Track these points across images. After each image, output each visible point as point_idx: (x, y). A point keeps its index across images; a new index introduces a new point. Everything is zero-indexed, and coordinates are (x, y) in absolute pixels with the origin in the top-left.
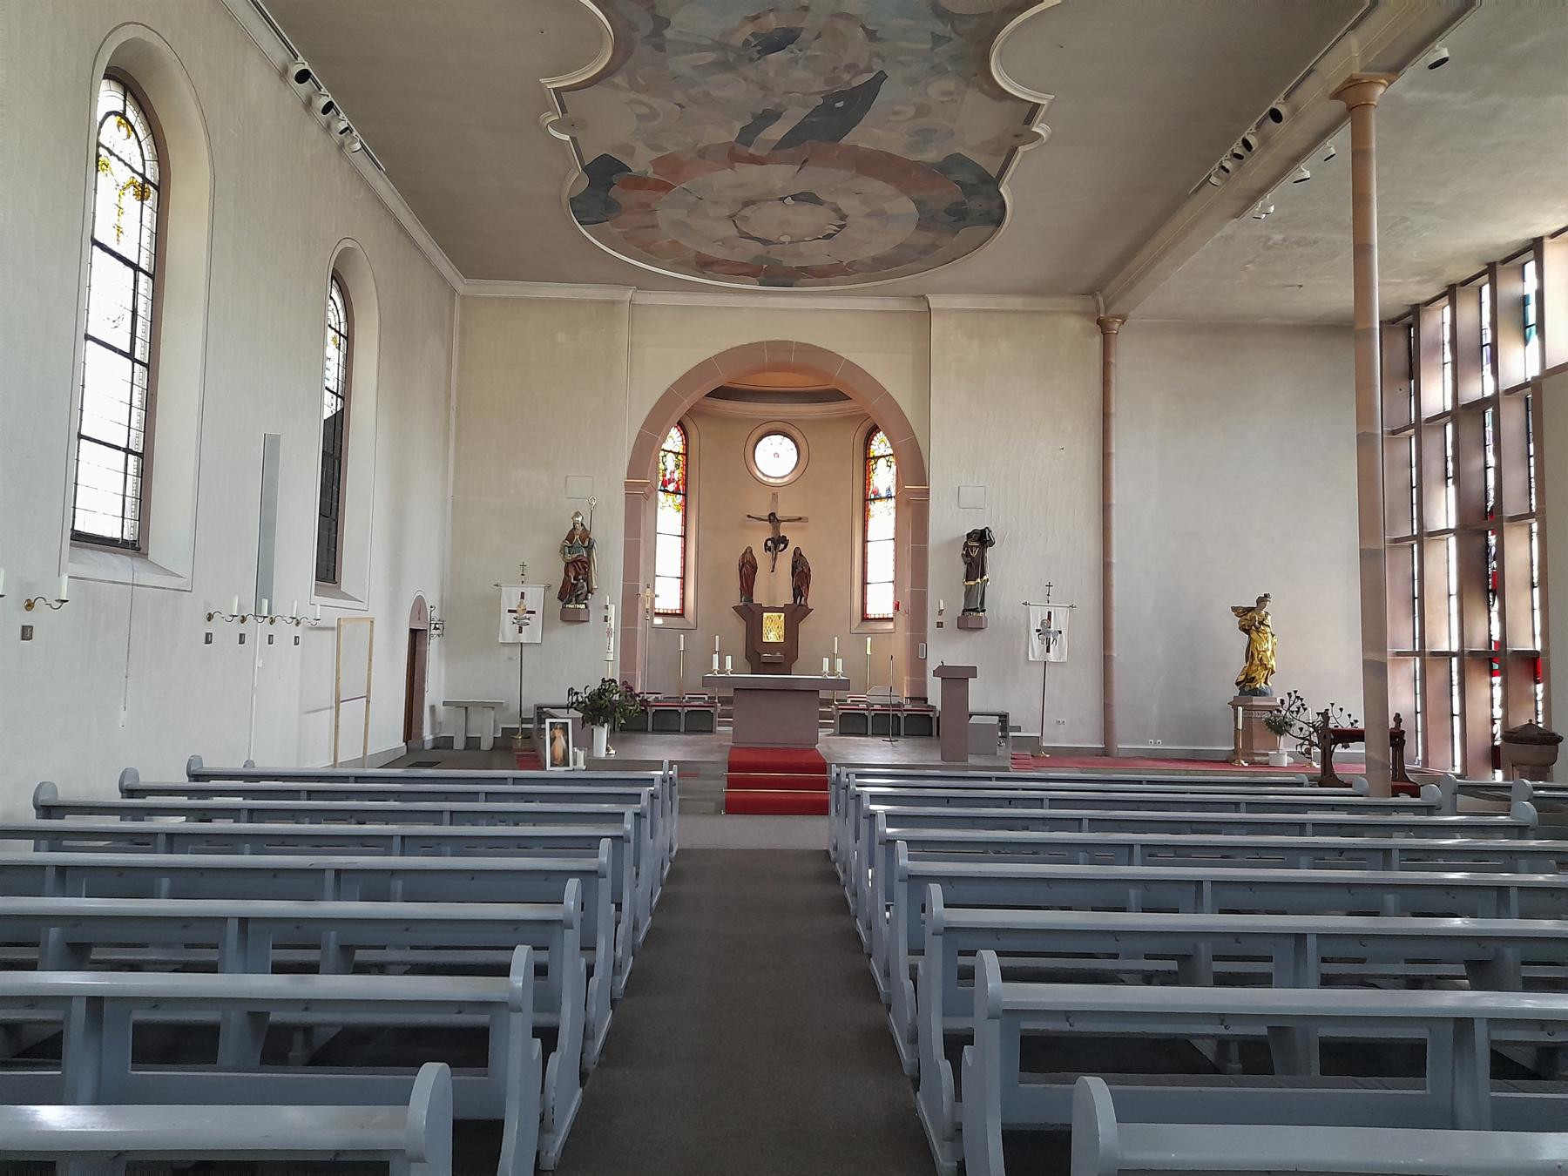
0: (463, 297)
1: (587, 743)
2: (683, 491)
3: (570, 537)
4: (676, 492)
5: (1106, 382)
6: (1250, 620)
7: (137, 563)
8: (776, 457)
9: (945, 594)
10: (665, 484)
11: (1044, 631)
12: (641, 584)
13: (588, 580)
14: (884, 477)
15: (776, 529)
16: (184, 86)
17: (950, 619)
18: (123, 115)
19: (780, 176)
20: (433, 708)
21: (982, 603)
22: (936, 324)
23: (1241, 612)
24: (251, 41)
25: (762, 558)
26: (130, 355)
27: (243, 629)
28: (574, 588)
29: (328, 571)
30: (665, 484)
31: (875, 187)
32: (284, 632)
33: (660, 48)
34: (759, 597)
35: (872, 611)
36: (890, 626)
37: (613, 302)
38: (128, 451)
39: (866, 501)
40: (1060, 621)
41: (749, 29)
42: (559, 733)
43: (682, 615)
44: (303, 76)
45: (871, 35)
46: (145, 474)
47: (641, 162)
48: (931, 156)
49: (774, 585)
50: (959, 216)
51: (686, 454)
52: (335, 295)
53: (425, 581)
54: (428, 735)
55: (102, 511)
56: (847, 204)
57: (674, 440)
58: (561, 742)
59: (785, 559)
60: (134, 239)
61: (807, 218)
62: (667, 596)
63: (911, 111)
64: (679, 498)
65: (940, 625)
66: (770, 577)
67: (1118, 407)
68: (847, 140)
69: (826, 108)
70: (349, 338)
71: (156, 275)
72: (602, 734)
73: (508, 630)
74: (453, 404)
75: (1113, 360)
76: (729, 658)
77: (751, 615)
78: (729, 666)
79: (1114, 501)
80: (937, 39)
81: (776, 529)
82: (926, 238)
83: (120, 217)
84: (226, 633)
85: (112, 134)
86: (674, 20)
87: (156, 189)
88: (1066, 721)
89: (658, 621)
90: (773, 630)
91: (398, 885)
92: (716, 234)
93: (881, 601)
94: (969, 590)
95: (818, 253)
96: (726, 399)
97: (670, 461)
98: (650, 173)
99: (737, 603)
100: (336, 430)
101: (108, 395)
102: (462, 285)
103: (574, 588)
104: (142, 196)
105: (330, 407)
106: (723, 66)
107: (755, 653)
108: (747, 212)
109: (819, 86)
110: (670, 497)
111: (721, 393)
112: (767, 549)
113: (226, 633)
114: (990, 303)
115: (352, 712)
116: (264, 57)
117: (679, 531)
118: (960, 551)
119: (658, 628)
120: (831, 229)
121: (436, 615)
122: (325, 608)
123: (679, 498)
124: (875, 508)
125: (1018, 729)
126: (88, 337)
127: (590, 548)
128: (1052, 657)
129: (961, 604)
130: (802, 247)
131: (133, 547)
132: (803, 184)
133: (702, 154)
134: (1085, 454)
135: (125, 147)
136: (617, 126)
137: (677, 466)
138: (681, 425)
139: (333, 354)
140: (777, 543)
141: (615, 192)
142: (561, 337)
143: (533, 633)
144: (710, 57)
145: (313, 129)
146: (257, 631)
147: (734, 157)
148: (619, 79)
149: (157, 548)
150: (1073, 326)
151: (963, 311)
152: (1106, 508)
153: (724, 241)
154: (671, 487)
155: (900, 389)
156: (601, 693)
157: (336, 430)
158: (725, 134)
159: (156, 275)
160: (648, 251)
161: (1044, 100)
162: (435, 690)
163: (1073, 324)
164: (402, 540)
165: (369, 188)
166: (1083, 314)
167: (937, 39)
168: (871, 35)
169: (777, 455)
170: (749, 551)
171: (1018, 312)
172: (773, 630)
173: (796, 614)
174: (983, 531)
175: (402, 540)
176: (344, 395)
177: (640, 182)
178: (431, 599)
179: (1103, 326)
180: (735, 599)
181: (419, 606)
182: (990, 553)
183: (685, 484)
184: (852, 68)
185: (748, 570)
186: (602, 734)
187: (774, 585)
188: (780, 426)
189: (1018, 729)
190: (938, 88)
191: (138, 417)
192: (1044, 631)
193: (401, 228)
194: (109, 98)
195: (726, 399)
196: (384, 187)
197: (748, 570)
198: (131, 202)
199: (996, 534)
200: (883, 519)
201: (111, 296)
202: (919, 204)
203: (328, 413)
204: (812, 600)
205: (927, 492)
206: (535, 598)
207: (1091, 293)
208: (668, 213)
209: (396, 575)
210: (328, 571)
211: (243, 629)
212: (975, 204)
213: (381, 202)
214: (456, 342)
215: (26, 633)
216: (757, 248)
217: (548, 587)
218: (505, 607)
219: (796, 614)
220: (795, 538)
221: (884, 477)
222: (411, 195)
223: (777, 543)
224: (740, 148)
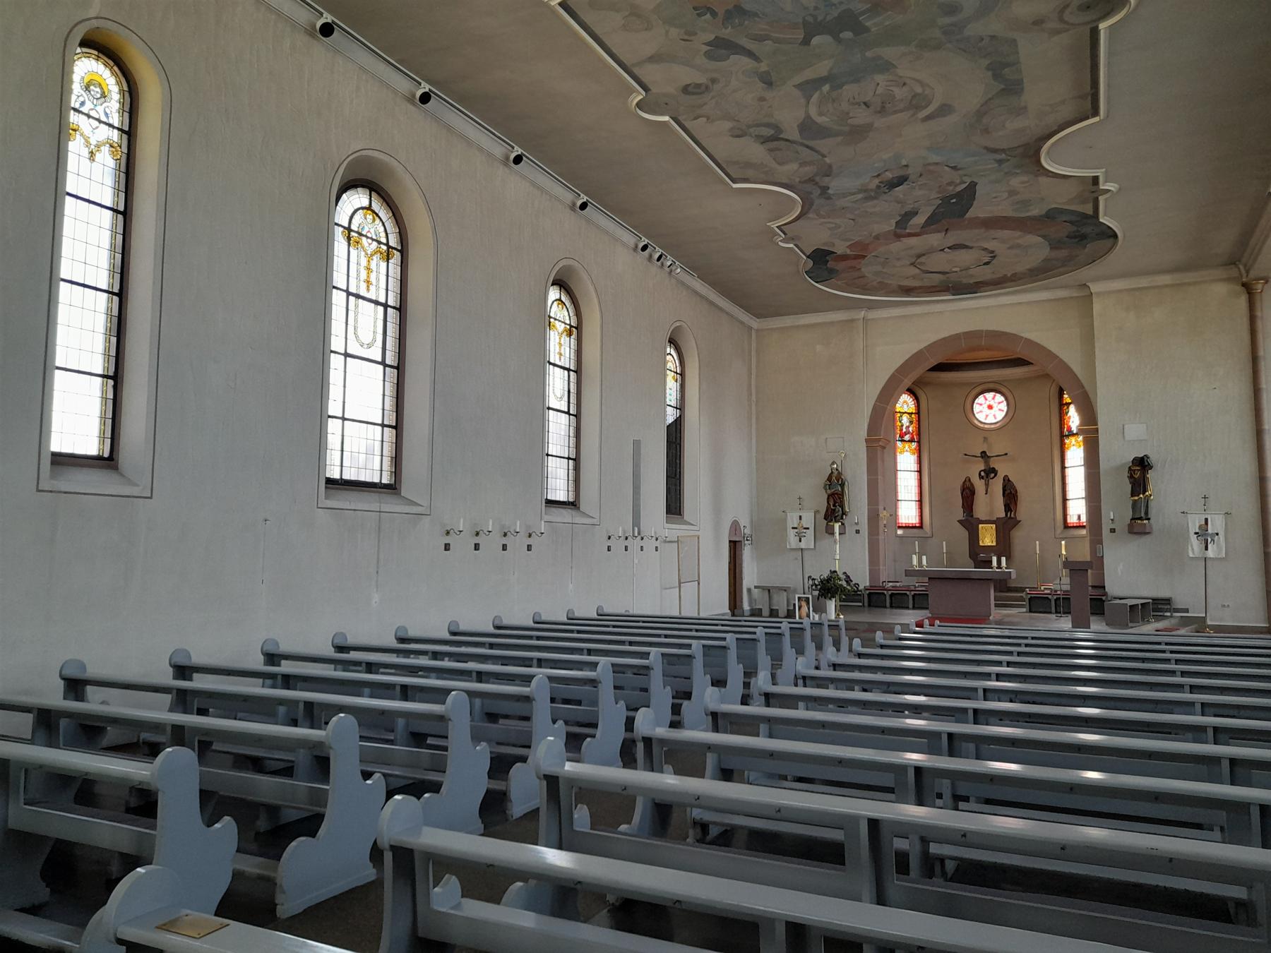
0: (757, 330)
1: (820, 609)
2: (918, 439)
3: (829, 479)
4: (911, 441)
7: (574, 512)
8: (990, 409)
9: (1117, 508)
10: (902, 436)
12: (881, 508)
13: (842, 506)
14: (1074, 419)
16: (584, 276)
18: (560, 300)
19: (935, 239)
20: (749, 590)
21: (1146, 513)
22: (1097, 307)
24: (617, 240)
25: (979, 485)
26: (568, 413)
28: (835, 509)
29: (674, 507)
30: (902, 436)
31: (1006, 233)
32: (650, 544)
33: (829, 198)
34: (980, 511)
35: (1072, 519)
36: (1084, 532)
37: (852, 321)
38: (569, 458)
39: (1063, 437)
40: (1216, 524)
41: (876, 181)
42: (804, 604)
43: (921, 527)
44: (644, 248)
45: (954, 168)
46: (577, 469)
47: (841, 248)
48: (1035, 211)
49: (990, 503)
50: (1081, 238)
51: (918, 413)
52: (673, 352)
53: (739, 509)
54: (746, 607)
55: (559, 489)
56: (991, 245)
57: (906, 403)
58: (805, 609)
59: (997, 486)
60: (567, 359)
61: (964, 257)
62: (908, 513)
63: (1005, 195)
64: (914, 445)
65: (1113, 531)
66: (987, 497)
68: (968, 215)
69: (946, 200)
70: (682, 374)
71: (578, 371)
72: (831, 605)
73: (792, 540)
74: (754, 398)
75: (1259, 314)
76: (924, 558)
77: (971, 524)
78: (924, 562)
79: (1266, 427)
80: (1000, 162)
81: (987, 463)
82: (1063, 253)
83: (559, 347)
84: (618, 545)
85: (556, 311)
86: (831, 185)
87: (576, 330)
89: (900, 532)
90: (988, 537)
92: (904, 273)
93: (1077, 509)
94: (1135, 504)
95: (986, 273)
96: (945, 373)
97: (905, 420)
98: (848, 252)
99: (961, 518)
100: (675, 434)
101: (558, 429)
102: (755, 323)
103: (835, 509)
104: (570, 335)
105: (671, 415)
106: (867, 199)
107: (978, 555)
108: (922, 259)
109: (934, 195)
110: (907, 445)
111: (940, 367)
112: (981, 477)
113: (618, 545)
114: (1144, 282)
115: (689, 589)
116: (624, 244)
117: (915, 467)
118: (1126, 474)
119: (901, 537)
120: (987, 260)
121: (747, 531)
122: (674, 530)
123: (914, 445)
124: (1070, 441)
126: (549, 408)
127: (842, 485)
128: (1211, 553)
129: (1129, 514)
130: (971, 272)
132: (953, 238)
133: (877, 238)
134: (1238, 389)
135: (560, 314)
136: (818, 234)
137: (911, 422)
138: (911, 391)
139: (672, 386)
140: (989, 473)
141: (831, 264)
142: (819, 348)
144: (860, 196)
145: (654, 268)
146: (635, 544)
147: (898, 236)
148: (810, 215)
149: (583, 506)
150: (1219, 293)
151: (1120, 291)
153: (914, 277)
154: (907, 438)
155: (1071, 356)
156: (829, 580)
157: (675, 434)
158: (890, 226)
159: (578, 371)
160: (865, 290)
161: (1099, 173)
162: (750, 578)
163: (1221, 289)
164: (723, 485)
165: (688, 287)
166: (1229, 280)
167: (1000, 162)
168: (954, 168)
169: (990, 407)
170: (968, 480)
171: (1167, 286)
172: (988, 537)
173: (1006, 526)
174: (1142, 459)
175: (723, 485)
176: (681, 407)
177: (844, 257)
178: (744, 522)
179: (1248, 288)
180: (960, 514)
181: (735, 526)
182: (1150, 474)
183: (919, 434)
184: (950, 184)
185: (968, 494)
186: (831, 605)
187: (990, 503)
188: (991, 386)
190: (1016, 182)
191: (573, 440)
192: (1203, 534)
193: (712, 303)
194: (554, 294)
195: (945, 373)
196: (698, 285)
197: (968, 494)
198: (565, 339)
199: (1153, 459)
200: (1075, 454)
201: (557, 386)
202: (1044, 237)
203: (670, 420)
204: (1023, 511)
205: (1097, 430)
206: (808, 519)
207: (1232, 262)
208: (868, 269)
209: (717, 510)
210: (674, 507)
211: (626, 543)
212: (1087, 230)
213: (696, 293)
216: (941, 276)
217: (816, 512)
218: (790, 525)
219: (1006, 526)
220: (1003, 469)
221: (1074, 419)
222: (713, 284)
223: (989, 473)
224: (899, 231)
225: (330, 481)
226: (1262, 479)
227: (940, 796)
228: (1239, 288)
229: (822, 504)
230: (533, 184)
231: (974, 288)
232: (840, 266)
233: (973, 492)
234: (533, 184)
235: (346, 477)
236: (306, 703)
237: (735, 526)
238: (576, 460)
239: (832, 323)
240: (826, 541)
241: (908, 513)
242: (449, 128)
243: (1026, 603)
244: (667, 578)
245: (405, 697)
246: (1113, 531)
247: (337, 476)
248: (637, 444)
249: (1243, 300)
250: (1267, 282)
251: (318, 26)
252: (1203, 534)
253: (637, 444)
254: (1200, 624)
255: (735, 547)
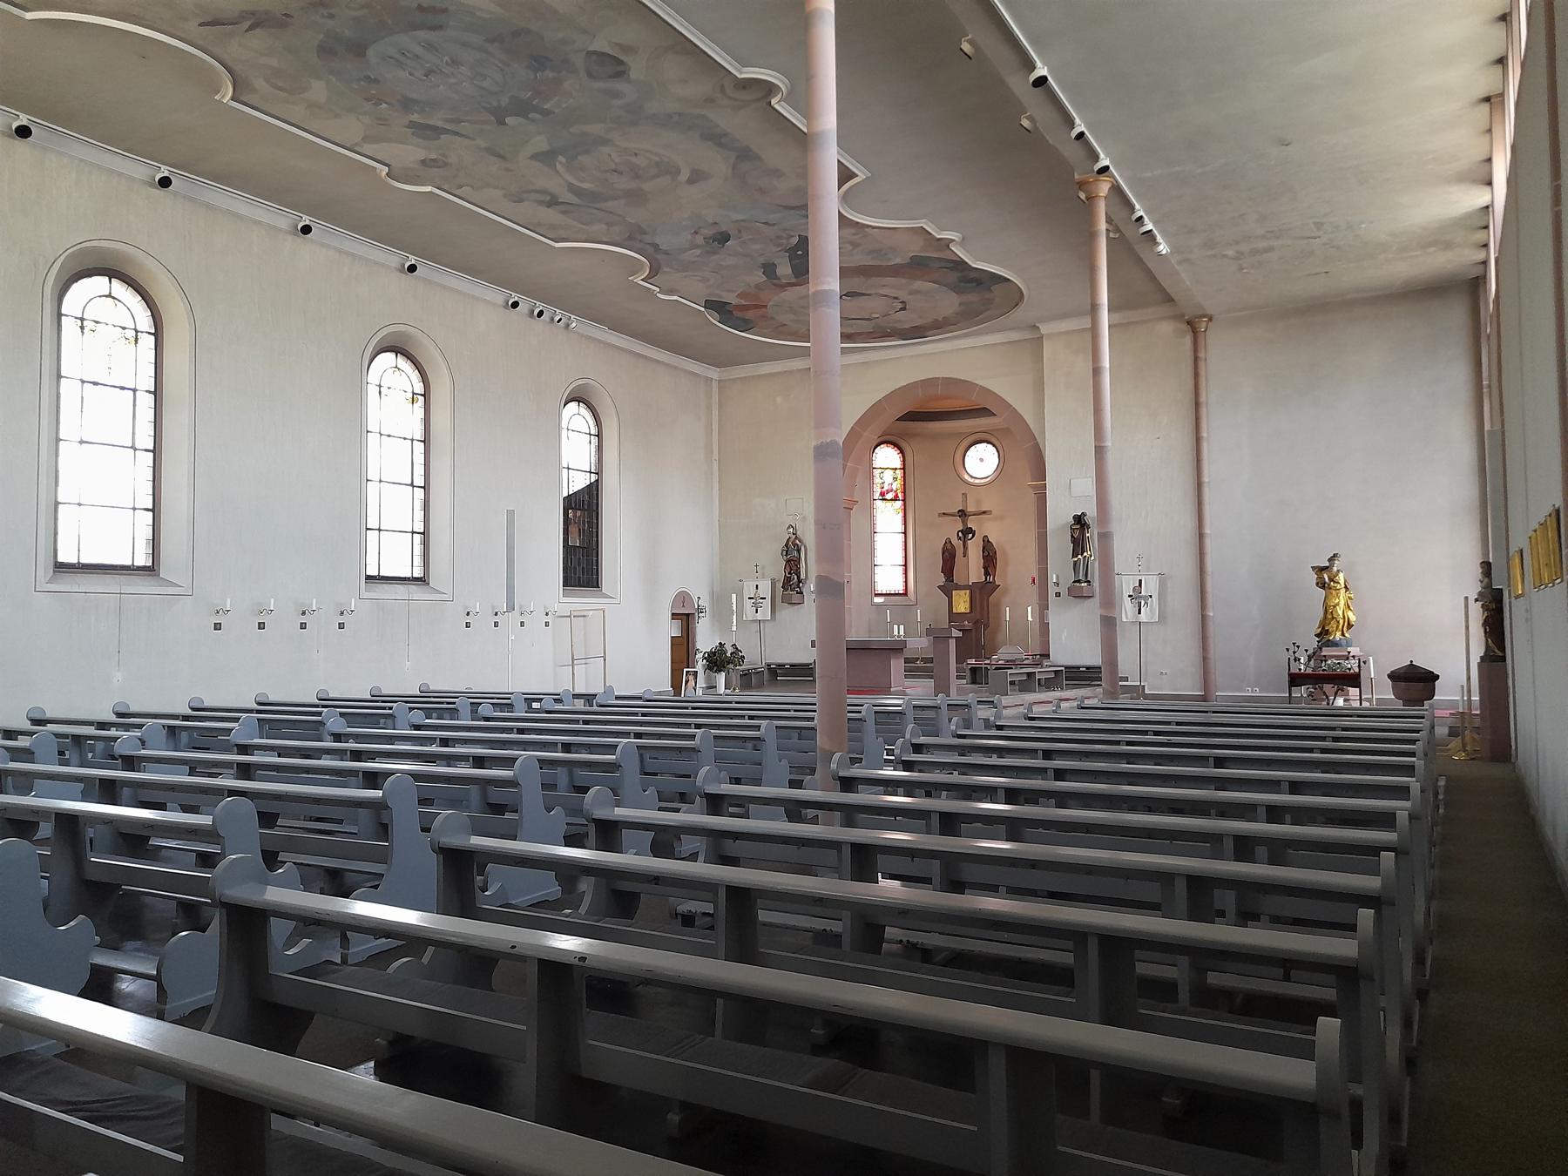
2: (904, 496)
4: (896, 499)
5: (1196, 375)
6: (1325, 576)
8: (981, 461)
10: (882, 494)
11: (1136, 596)
15: (965, 523)
16: (426, 341)
17: (1063, 590)
22: (1048, 348)
23: (1320, 570)
27: (548, 619)
28: (791, 584)
40: (1151, 587)
43: (905, 594)
46: (426, 544)
49: (972, 569)
56: (903, 295)
59: (975, 547)
62: (889, 578)
64: (899, 504)
65: (1058, 595)
66: (962, 563)
67: (1210, 395)
81: (965, 523)
88: (1160, 664)
89: (878, 600)
91: (1272, 904)
95: (907, 320)
102: (714, 373)
110: (889, 504)
111: (911, 416)
117: (901, 528)
119: (878, 605)
123: (899, 504)
125: (1126, 679)
127: (799, 551)
128: (1143, 617)
131: (422, 581)
137: (895, 479)
140: (967, 532)
142: (779, 400)
143: (765, 612)
146: (514, 617)
151: (1067, 332)
152: (1199, 485)
163: (1167, 328)
164: (669, 549)
183: (904, 492)
185: (949, 559)
187: (972, 569)
189: (1126, 679)
191: (419, 515)
206: (765, 589)
214: (715, 413)
215: (496, 624)
225: (369, 578)
226: (1201, 536)
227: (1222, 914)
228: (1185, 327)
229: (778, 570)
230: (340, 251)
231: (916, 333)
232: (749, 315)
233: (953, 556)
234: (340, 251)
235: (83, 561)
236: (853, 845)
237: (683, 597)
238: (425, 534)
239: (791, 372)
240: (786, 613)
241: (889, 578)
242: (209, 207)
243: (968, 673)
244: (616, 650)
245: (849, 823)
246: (1058, 595)
247: (372, 571)
248: (511, 513)
249: (1188, 339)
250: (1210, 320)
251: (14, 126)
252: (1136, 596)
253: (511, 513)
254: (1138, 691)
255: (686, 620)
